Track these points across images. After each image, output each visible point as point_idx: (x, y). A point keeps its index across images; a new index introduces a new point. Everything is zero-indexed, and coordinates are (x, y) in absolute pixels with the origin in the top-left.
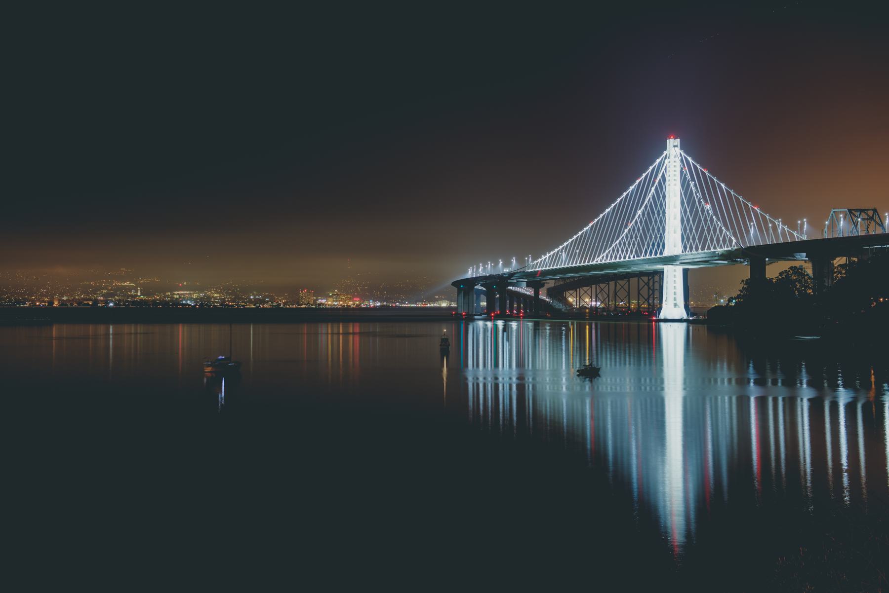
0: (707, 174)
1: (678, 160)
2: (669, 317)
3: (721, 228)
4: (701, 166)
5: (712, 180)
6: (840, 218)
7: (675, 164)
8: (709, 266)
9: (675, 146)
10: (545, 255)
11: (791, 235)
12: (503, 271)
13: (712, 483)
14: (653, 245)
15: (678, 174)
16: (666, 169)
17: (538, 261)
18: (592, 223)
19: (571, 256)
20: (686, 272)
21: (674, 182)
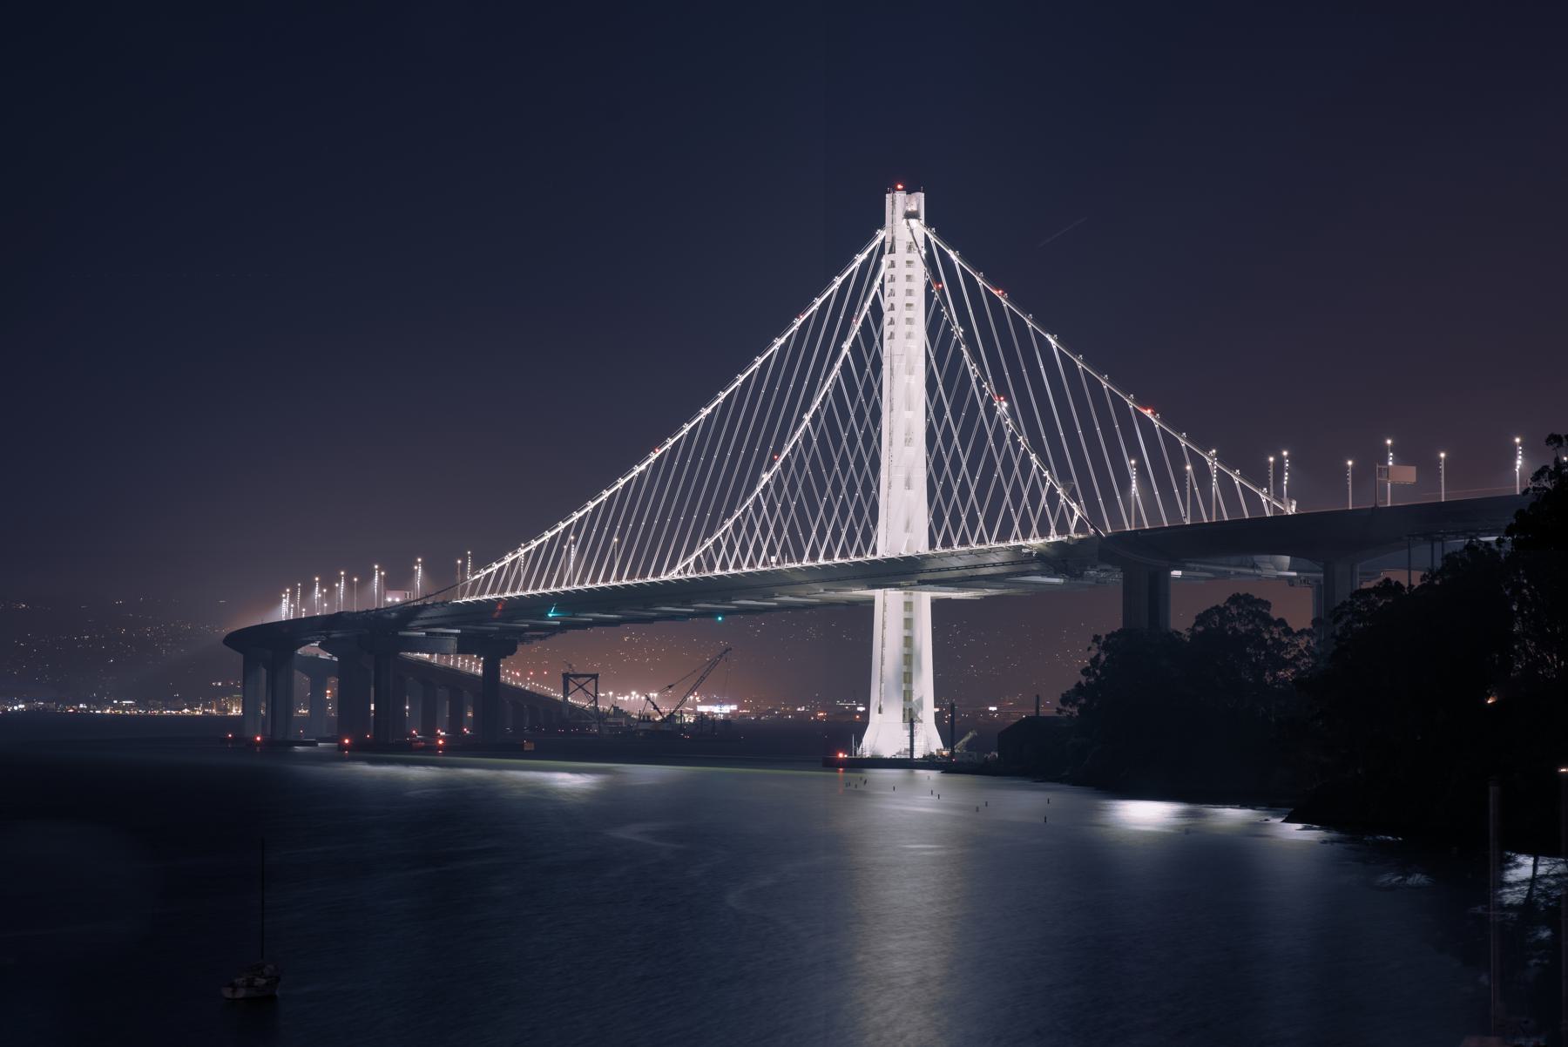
0: (1005, 303)
1: (918, 258)
3: (1052, 489)
5: (1095, 386)
7: (909, 271)
8: (1012, 591)
9: (910, 215)
10: (514, 550)
11: (1253, 500)
12: (385, 602)
14: (844, 512)
15: (919, 300)
16: (882, 287)
17: (489, 571)
18: (659, 452)
19: (594, 556)
21: (907, 328)
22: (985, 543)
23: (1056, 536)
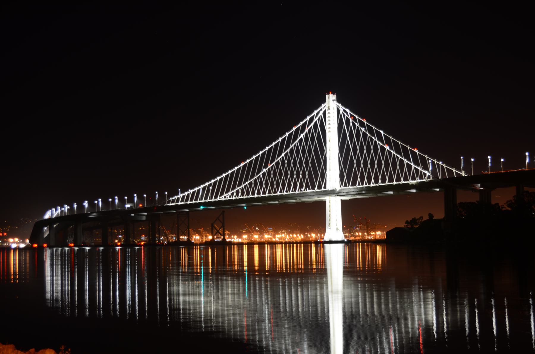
2: (334, 240)
4: (359, 116)
6: (135, 197)
13: (263, 341)
20: (343, 202)
22: (288, 192)
23: (388, 183)
